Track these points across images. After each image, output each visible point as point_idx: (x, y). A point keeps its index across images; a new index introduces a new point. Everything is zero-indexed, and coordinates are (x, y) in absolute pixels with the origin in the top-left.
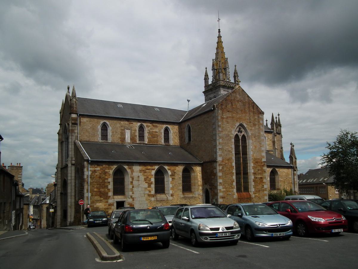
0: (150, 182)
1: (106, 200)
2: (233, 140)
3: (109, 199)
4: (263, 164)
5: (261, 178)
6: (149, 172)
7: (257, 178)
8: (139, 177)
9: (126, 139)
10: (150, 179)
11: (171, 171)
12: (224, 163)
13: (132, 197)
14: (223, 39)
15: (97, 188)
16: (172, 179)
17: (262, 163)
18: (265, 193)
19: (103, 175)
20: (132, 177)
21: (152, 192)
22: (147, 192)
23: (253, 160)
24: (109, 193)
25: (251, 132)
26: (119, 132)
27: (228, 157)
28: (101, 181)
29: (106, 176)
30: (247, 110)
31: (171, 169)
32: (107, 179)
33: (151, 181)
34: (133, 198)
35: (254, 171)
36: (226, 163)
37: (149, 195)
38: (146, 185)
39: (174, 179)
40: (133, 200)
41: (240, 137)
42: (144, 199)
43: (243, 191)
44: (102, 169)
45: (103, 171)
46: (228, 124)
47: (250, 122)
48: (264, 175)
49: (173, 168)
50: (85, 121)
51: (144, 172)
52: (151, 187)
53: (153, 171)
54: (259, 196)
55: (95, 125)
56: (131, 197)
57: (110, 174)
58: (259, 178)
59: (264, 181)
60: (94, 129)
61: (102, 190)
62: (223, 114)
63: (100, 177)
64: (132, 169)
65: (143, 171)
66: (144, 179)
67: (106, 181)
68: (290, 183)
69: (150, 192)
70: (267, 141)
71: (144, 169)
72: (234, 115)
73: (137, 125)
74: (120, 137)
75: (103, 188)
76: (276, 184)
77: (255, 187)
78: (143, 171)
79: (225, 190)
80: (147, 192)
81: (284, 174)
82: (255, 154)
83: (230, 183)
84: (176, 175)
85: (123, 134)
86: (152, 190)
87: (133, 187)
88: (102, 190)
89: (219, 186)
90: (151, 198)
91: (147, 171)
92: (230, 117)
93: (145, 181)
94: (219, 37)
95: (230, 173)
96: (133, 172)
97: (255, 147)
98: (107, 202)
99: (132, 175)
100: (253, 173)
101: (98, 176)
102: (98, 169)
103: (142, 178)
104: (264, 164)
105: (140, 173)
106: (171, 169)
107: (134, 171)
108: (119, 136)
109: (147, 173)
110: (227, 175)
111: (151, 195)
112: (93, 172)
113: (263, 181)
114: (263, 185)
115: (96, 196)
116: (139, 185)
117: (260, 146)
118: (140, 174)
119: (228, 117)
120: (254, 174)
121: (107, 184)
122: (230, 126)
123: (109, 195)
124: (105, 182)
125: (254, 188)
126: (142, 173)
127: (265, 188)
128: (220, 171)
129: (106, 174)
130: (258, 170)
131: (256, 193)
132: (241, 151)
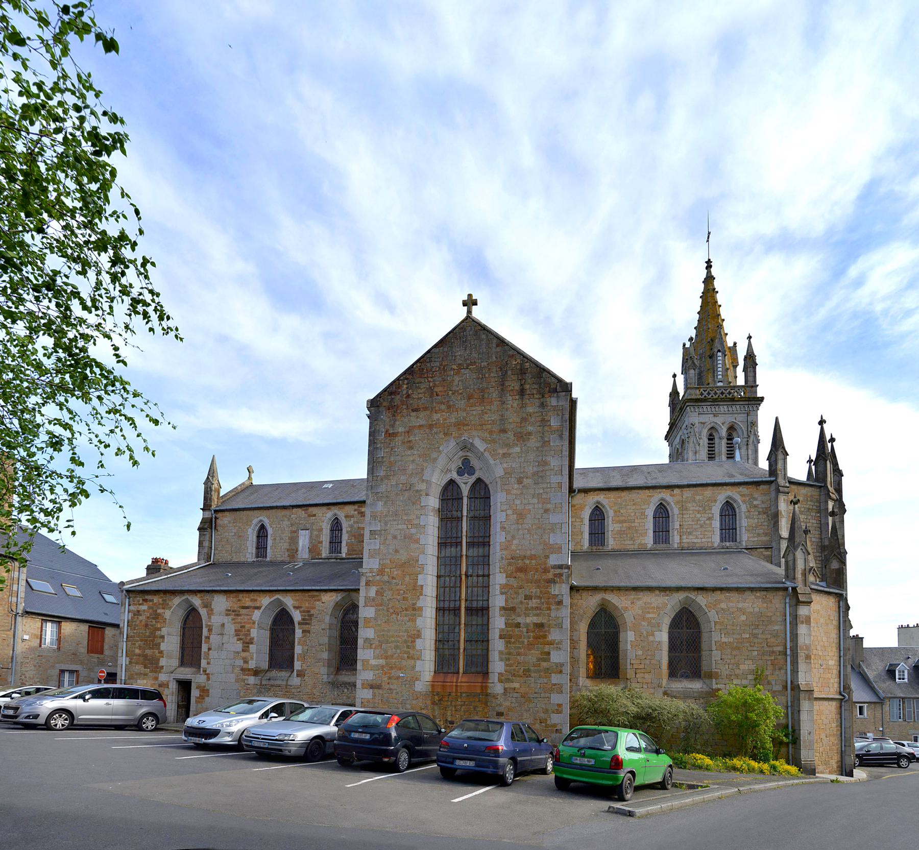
0: (249, 638)
1: (155, 675)
2: (433, 502)
3: (160, 672)
4: (550, 576)
5: (541, 626)
6: (247, 615)
7: (518, 625)
8: (223, 625)
9: (299, 552)
10: (249, 631)
11: (300, 612)
12: (386, 578)
13: (206, 671)
14: (717, 284)
15: (140, 647)
16: (303, 631)
17: (546, 571)
18: (554, 682)
19: (151, 622)
20: (210, 625)
21: (250, 662)
22: (240, 662)
23: (505, 562)
24: (161, 659)
25: (505, 465)
26: (287, 538)
27: (403, 556)
28: (147, 634)
29: (158, 622)
30: (494, 393)
31: (301, 607)
32: (159, 629)
33: (250, 635)
34: (208, 674)
35: (506, 601)
36: (393, 578)
37: (242, 669)
38: (239, 646)
39: (309, 632)
40: (208, 679)
41: (465, 490)
42: (232, 677)
43: (461, 671)
44: (152, 608)
45: (154, 611)
46: (409, 452)
47: (504, 431)
48: (553, 614)
49: (307, 605)
50: (226, 522)
51: (235, 615)
52: (248, 651)
53: (256, 611)
54: (521, 691)
55: (242, 527)
56: (203, 671)
57: (166, 619)
58: (527, 625)
59: (554, 635)
60: (240, 536)
61: (149, 652)
62: (395, 421)
63: (146, 625)
64: (210, 607)
65: (233, 611)
66: (236, 630)
67: (158, 633)
68: (773, 652)
69: (246, 662)
70: (747, 517)
71: (236, 606)
72: (436, 416)
73: (325, 518)
74: (288, 548)
75: (150, 648)
76: (704, 658)
77: (506, 657)
78: (233, 611)
79: (382, 662)
80: (240, 662)
81: (743, 618)
82: (515, 542)
83: (405, 641)
84: (314, 621)
85: (294, 540)
86: (252, 659)
87: (209, 649)
88: (149, 652)
89: (364, 648)
90: (247, 677)
91: (243, 611)
92: (421, 426)
93: (237, 635)
94: (709, 280)
95: (406, 610)
96: (212, 614)
97: (521, 516)
98: (156, 678)
99: (210, 622)
100: (503, 609)
101: (143, 623)
102: (144, 607)
103: (230, 628)
104: (555, 575)
105: (226, 617)
106: (301, 607)
107: (214, 612)
108: (286, 546)
109: (242, 617)
110: (394, 616)
111: (249, 670)
112: (134, 615)
113: (545, 637)
114: (549, 653)
115: (137, 663)
116: (223, 644)
117: (542, 511)
118: (227, 620)
119: (414, 427)
120: (508, 610)
121: (159, 640)
122: (420, 456)
123: (161, 664)
124: (155, 637)
125: (501, 660)
126: (230, 618)
127: (556, 664)
128: (369, 602)
129: (158, 618)
130: (528, 597)
131: (508, 680)
132: (464, 533)
